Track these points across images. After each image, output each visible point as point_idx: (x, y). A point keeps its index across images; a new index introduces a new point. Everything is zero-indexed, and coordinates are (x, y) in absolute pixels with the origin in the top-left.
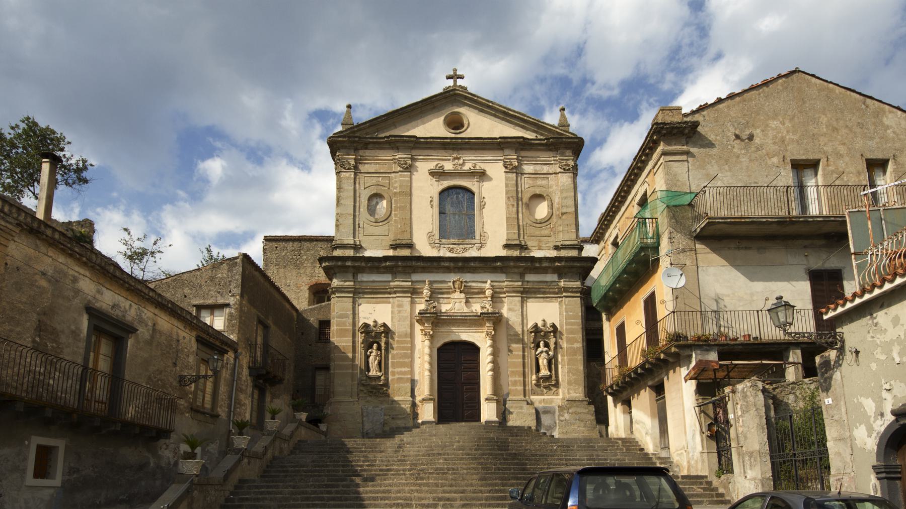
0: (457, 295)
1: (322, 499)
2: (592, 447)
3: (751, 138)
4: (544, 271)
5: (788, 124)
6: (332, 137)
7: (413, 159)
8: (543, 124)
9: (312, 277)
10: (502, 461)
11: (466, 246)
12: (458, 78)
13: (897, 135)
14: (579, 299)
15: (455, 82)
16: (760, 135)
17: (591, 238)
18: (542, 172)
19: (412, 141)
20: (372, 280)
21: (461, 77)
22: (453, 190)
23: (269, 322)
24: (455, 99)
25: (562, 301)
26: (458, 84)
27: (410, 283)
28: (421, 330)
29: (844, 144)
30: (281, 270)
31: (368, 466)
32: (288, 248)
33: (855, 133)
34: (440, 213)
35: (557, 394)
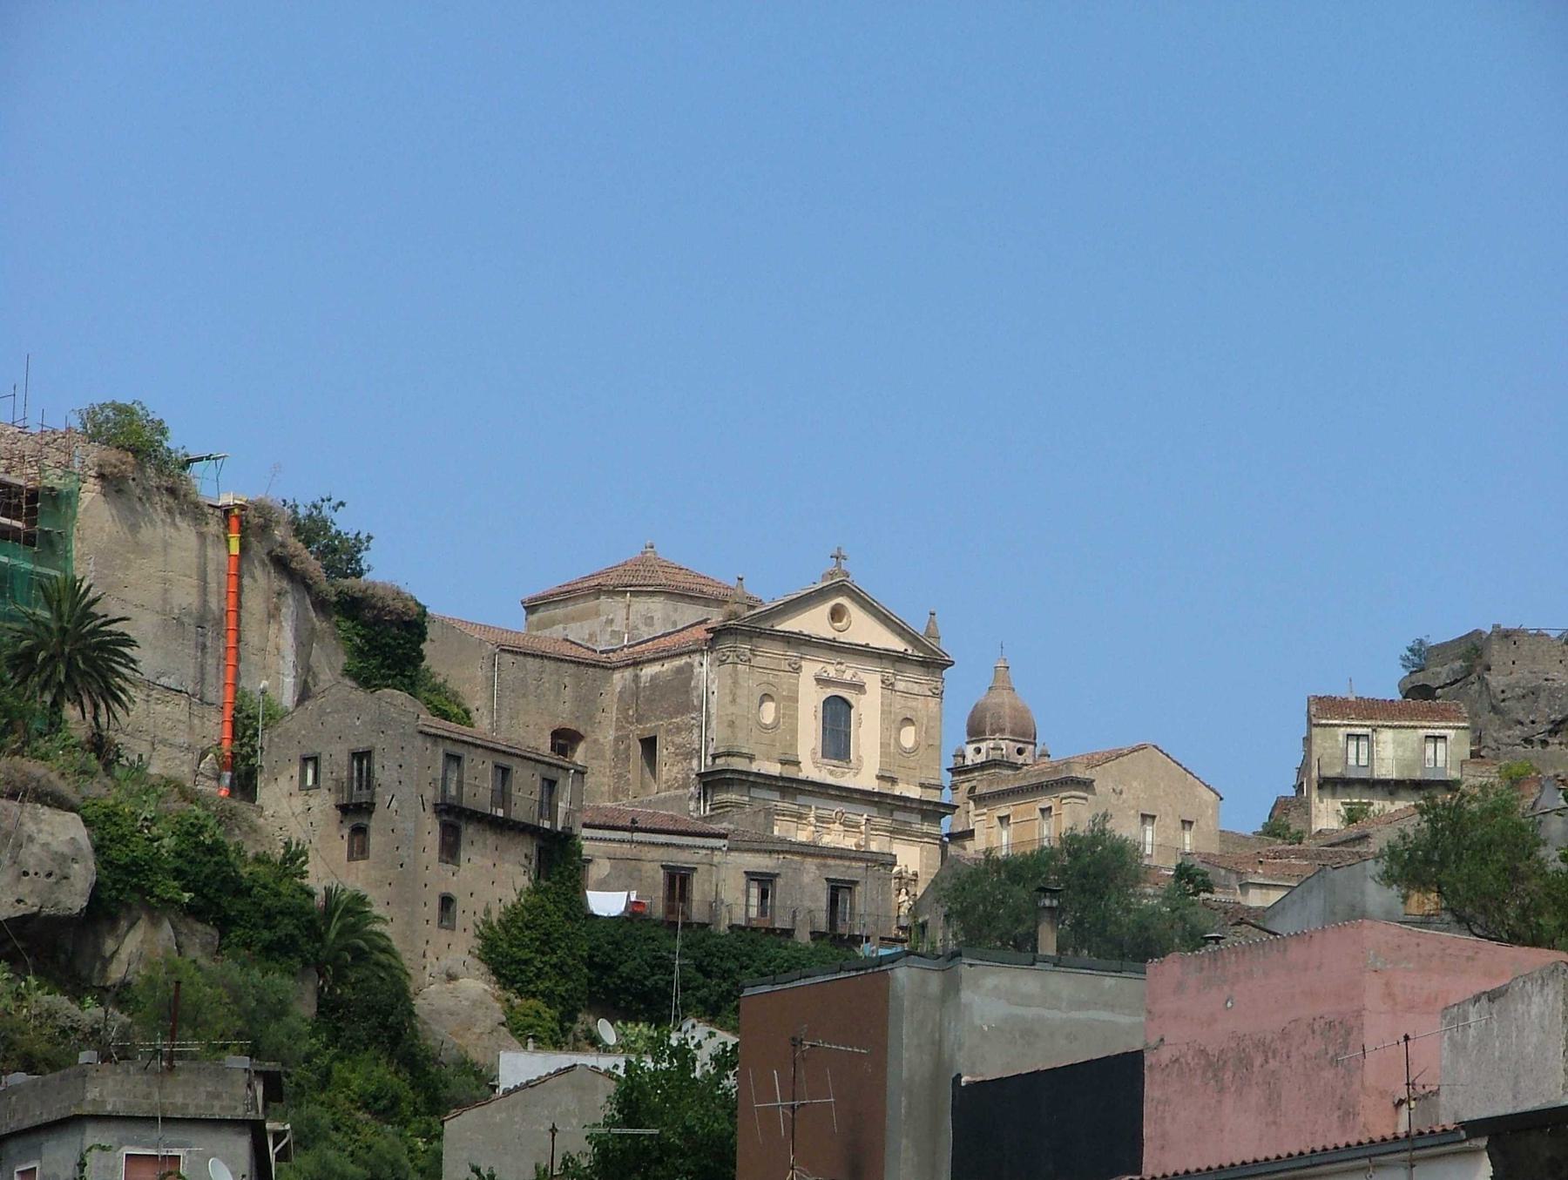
0: (837, 826)
3: (1121, 793)
4: (911, 810)
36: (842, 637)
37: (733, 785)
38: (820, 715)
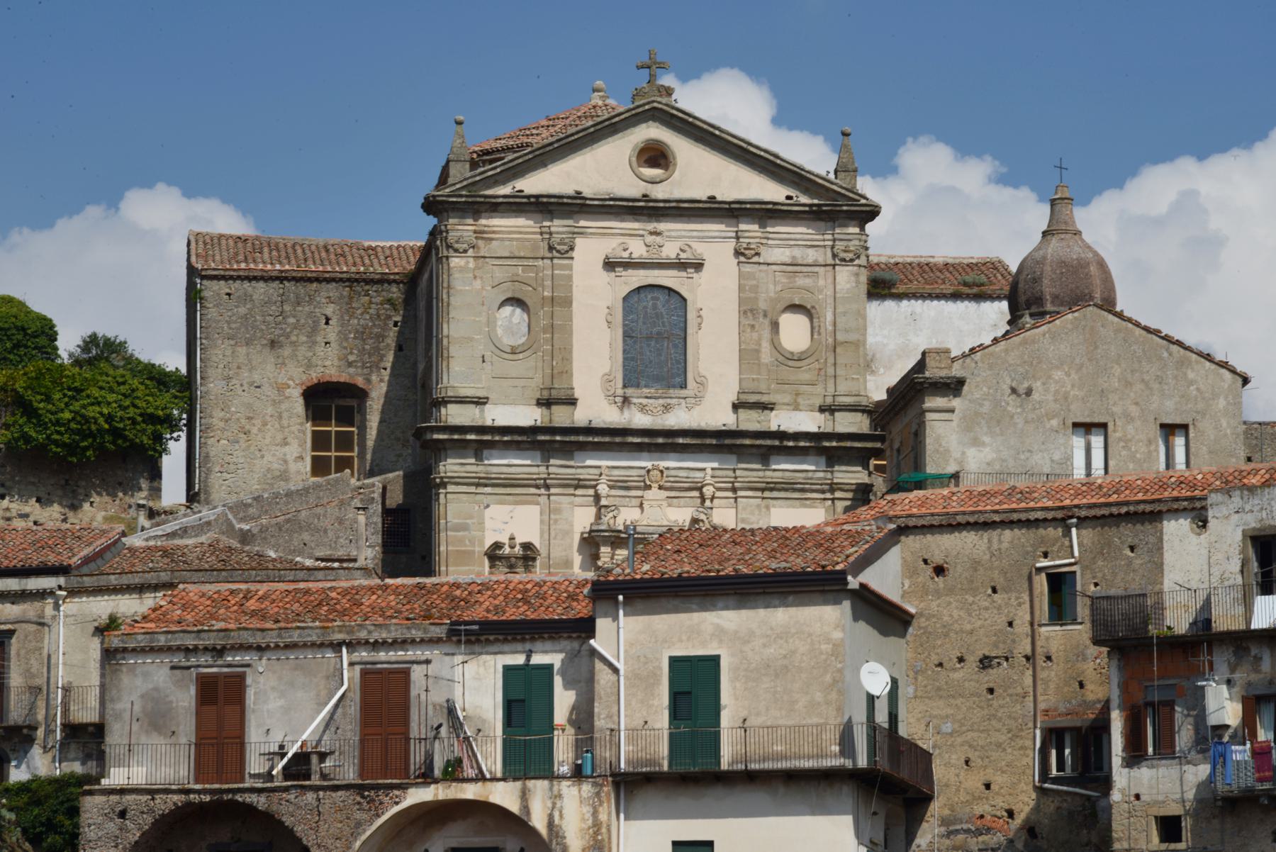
3: (1029, 392)
5: (1074, 376)
8: (808, 175)
9: (309, 366)
11: (669, 401)
13: (1201, 393)
16: (1040, 389)
18: (805, 263)
24: (653, 115)
29: (1137, 404)
30: (239, 349)
33: (1151, 389)
36: (659, 192)
37: (445, 449)
38: (691, 315)
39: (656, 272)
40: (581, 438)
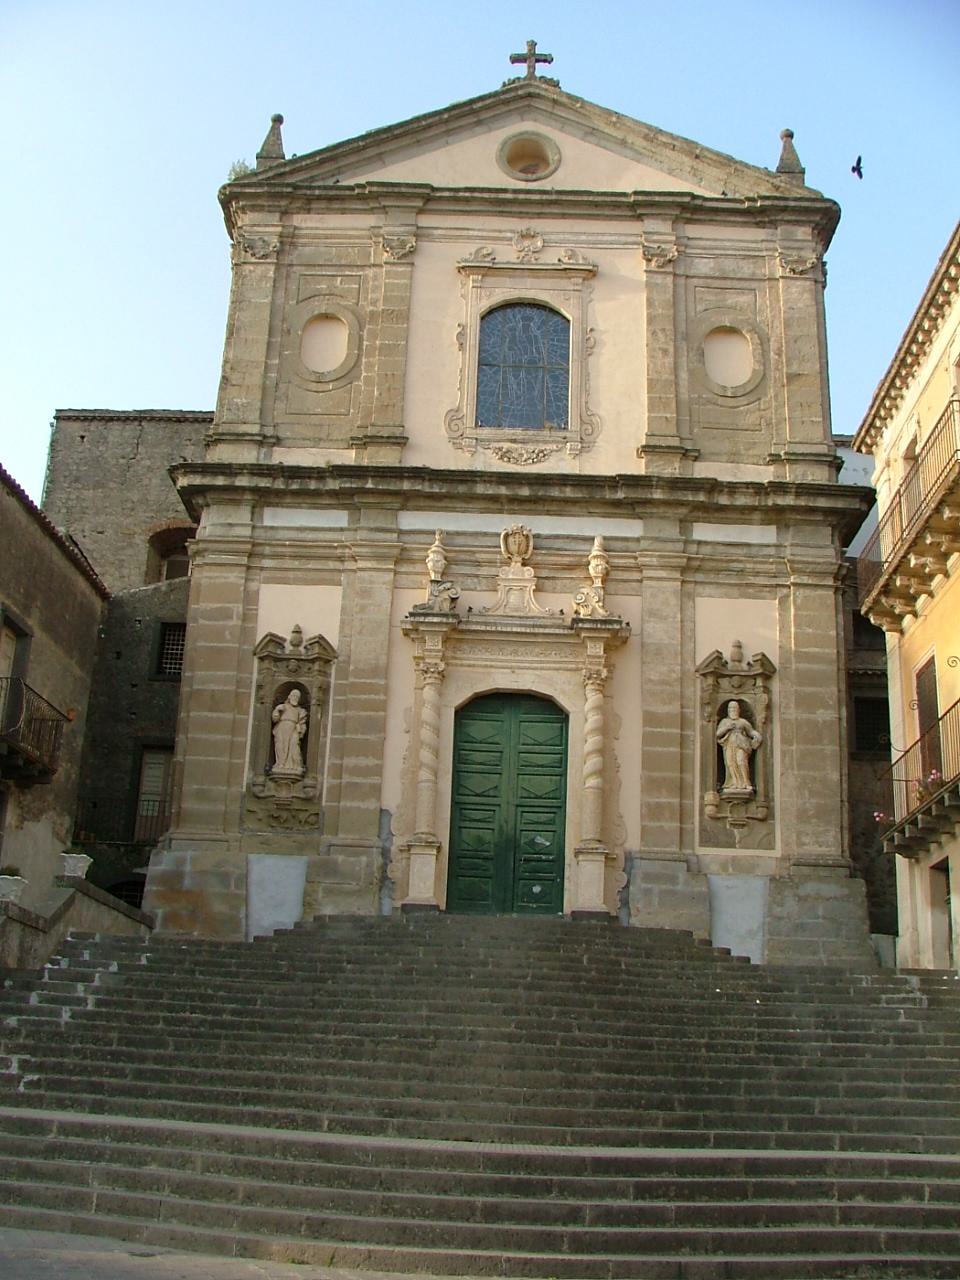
1: (96, 1088)
2: (838, 991)
4: (743, 515)
6: (229, 185)
7: (420, 234)
10: (586, 1020)
12: (538, 61)
14: (831, 593)
15: (532, 69)
17: (859, 434)
19: (418, 196)
20: (298, 525)
21: (546, 59)
22: (517, 310)
23: (30, 622)
25: (788, 596)
26: (538, 74)
27: (395, 535)
28: (415, 658)
31: (234, 1012)
32: (110, 438)
34: (481, 363)
35: (771, 846)
39: (529, 282)
40: (406, 485)
